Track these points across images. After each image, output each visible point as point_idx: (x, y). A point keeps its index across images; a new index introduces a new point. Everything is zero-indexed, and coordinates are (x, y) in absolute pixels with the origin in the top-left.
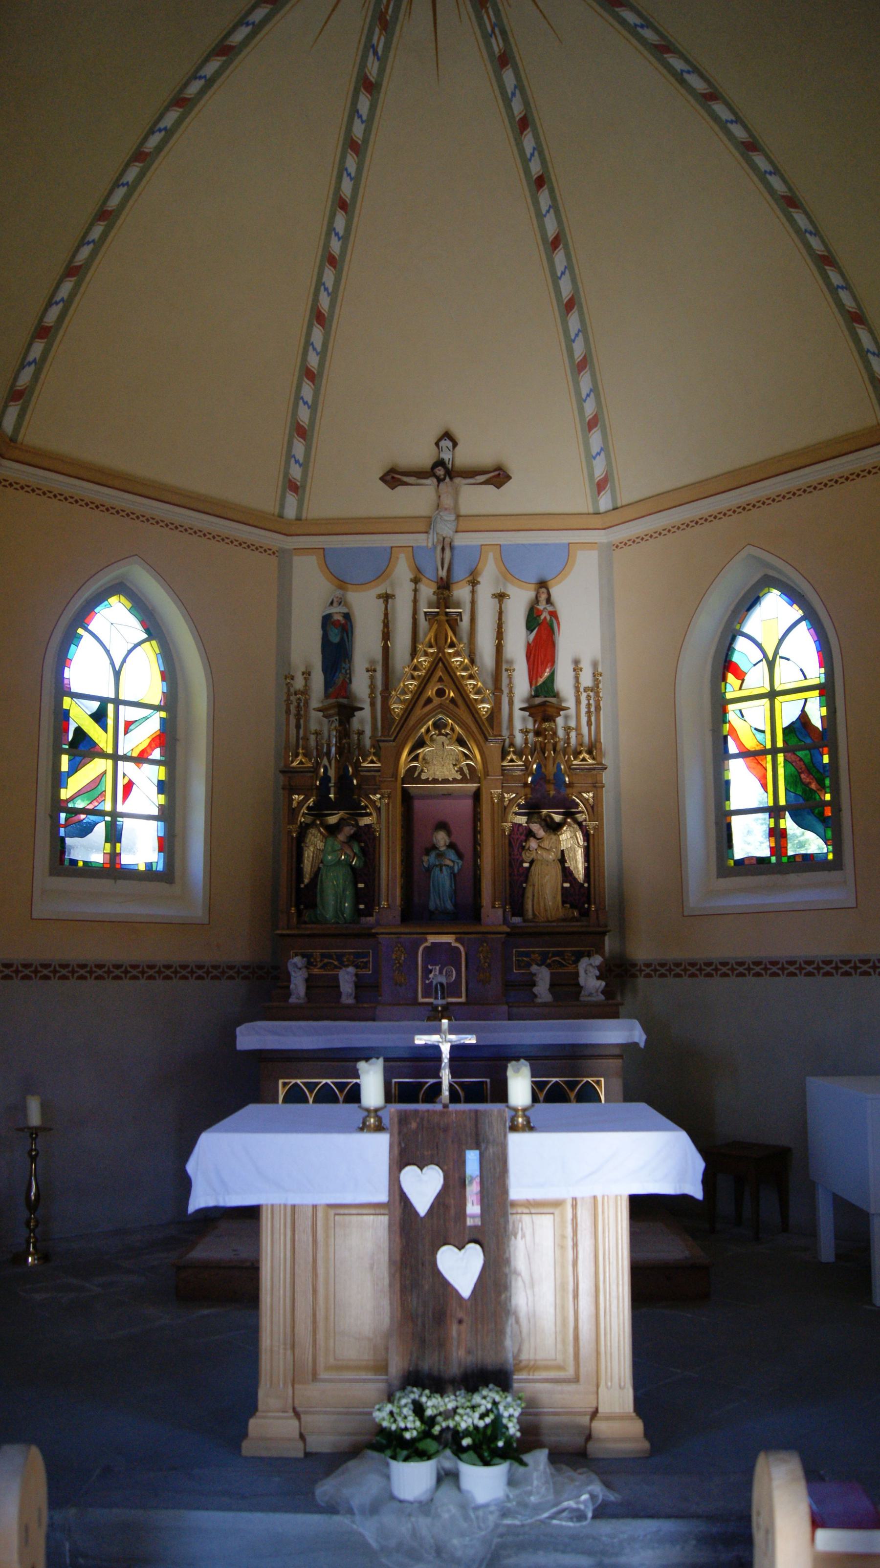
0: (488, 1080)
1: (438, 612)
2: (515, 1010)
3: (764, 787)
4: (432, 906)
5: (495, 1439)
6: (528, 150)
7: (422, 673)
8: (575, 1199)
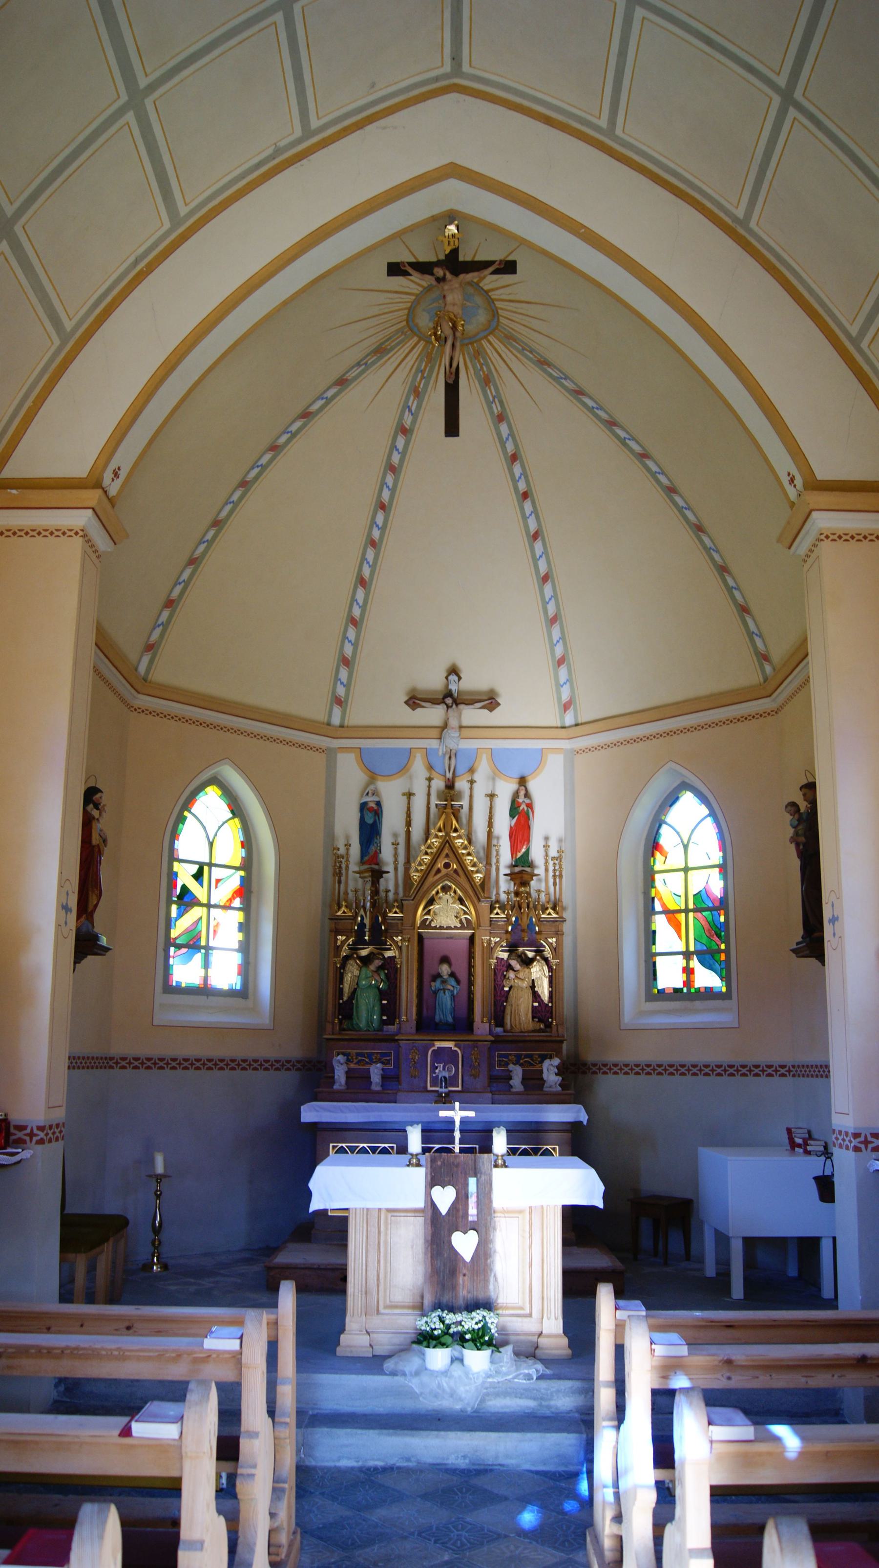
0: (477, 1146)
1: (446, 805)
2: (496, 1097)
3: (680, 937)
4: (437, 1019)
5: (483, 1335)
6: (517, 475)
7: (434, 850)
8: (531, 1208)
